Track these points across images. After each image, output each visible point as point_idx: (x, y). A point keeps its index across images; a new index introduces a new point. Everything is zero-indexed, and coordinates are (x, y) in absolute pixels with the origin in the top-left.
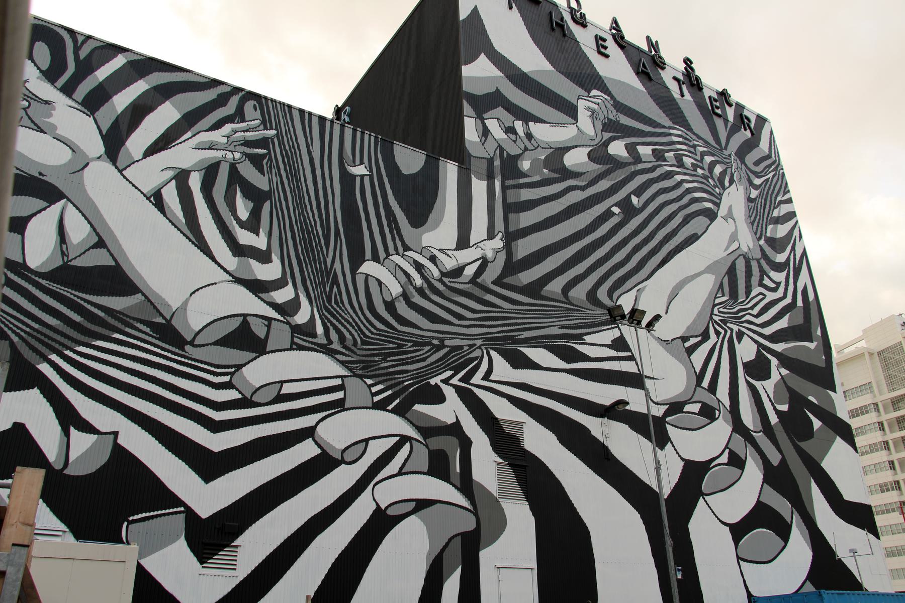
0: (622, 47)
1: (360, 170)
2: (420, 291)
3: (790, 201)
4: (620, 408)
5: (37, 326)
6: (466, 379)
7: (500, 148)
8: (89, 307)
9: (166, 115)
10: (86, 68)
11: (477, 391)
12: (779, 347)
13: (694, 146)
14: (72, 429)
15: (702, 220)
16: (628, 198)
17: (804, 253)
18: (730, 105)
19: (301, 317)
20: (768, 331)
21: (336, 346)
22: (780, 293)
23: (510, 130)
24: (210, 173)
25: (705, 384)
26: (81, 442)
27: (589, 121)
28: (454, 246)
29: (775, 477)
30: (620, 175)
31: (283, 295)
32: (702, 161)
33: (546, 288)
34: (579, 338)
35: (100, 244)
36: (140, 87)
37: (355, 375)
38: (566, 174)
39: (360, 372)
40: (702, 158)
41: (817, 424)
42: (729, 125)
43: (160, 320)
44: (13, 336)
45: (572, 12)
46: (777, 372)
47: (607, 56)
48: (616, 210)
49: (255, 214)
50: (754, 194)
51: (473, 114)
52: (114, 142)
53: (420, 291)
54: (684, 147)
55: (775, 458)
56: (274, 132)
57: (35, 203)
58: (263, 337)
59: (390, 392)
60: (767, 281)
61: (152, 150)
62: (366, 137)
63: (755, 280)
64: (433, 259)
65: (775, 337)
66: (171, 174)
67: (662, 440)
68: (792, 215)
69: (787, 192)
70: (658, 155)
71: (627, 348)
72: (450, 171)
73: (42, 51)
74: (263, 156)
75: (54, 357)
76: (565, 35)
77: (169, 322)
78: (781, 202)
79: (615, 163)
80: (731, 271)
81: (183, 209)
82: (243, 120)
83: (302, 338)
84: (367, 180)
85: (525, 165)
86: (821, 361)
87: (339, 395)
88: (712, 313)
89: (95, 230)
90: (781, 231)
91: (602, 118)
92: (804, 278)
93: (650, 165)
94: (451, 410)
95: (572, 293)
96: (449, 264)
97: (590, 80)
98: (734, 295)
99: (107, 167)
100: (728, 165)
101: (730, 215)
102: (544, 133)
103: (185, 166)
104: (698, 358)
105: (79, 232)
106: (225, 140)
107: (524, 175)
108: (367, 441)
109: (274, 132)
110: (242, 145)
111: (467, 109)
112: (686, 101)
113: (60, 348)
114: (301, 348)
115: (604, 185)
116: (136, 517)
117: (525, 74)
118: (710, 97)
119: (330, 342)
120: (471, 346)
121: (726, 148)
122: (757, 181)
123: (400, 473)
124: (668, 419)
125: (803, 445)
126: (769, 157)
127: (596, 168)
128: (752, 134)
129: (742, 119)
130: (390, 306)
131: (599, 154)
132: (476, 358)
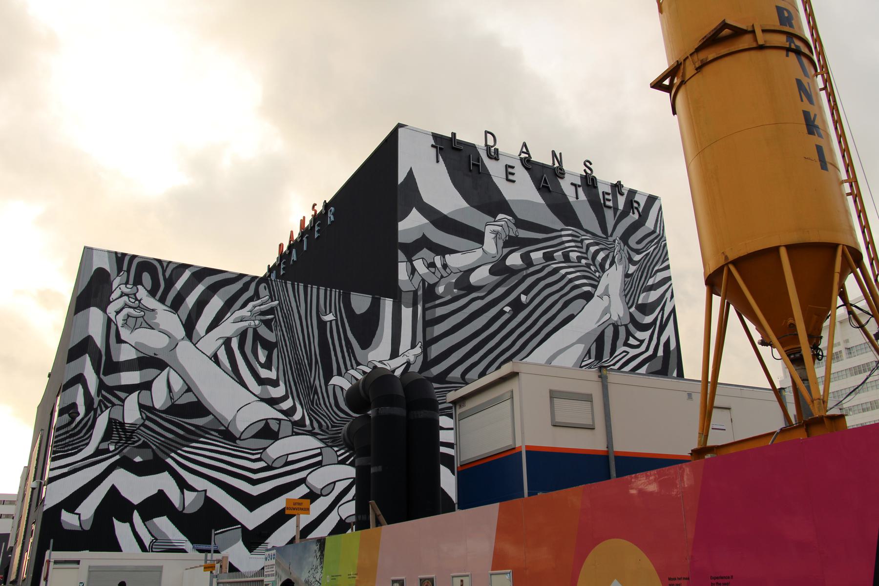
1: (329, 317)
7: (423, 281)
9: (216, 303)
10: (170, 283)
13: (582, 241)
15: (582, 301)
17: (673, 311)
19: (297, 417)
21: (317, 430)
22: (643, 348)
24: (243, 336)
26: (190, 496)
27: (493, 242)
31: (286, 405)
33: (450, 375)
35: (189, 390)
36: (200, 289)
37: (328, 446)
39: (330, 444)
40: (588, 249)
43: (223, 428)
48: (507, 309)
49: (269, 358)
50: (632, 269)
52: (189, 326)
54: (573, 244)
56: (277, 302)
57: (153, 372)
58: (276, 430)
61: (210, 329)
62: (333, 293)
66: (221, 341)
70: (548, 257)
72: (387, 305)
73: (146, 277)
75: (173, 455)
77: (227, 428)
79: (512, 271)
80: (600, 340)
82: (259, 298)
83: (298, 428)
84: (334, 323)
87: (319, 458)
91: (504, 236)
92: (669, 331)
98: (599, 356)
99: (187, 343)
101: (606, 293)
102: (456, 261)
103: (228, 335)
105: (178, 385)
106: (249, 314)
107: (440, 297)
108: (334, 483)
109: (277, 302)
111: (401, 256)
114: (298, 434)
115: (500, 291)
117: (445, 216)
119: (314, 429)
121: (611, 235)
122: (637, 258)
126: (654, 232)
127: (496, 279)
128: (640, 215)
131: (499, 268)
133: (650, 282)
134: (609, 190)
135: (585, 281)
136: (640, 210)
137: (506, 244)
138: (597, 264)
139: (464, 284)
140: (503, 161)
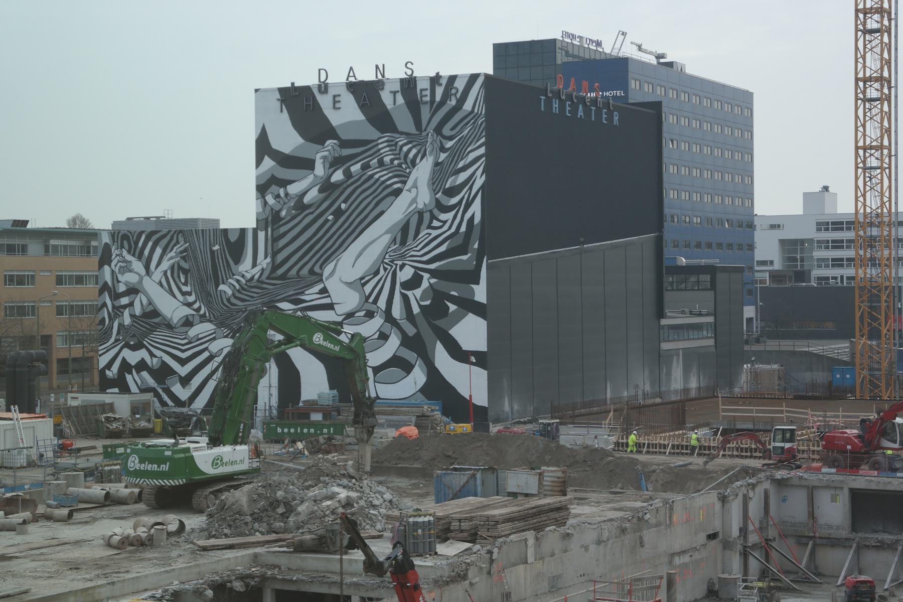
2: (239, 291)
7: (272, 209)
13: (396, 145)
19: (202, 312)
26: (155, 360)
29: (406, 341)
31: (196, 306)
34: (303, 293)
35: (150, 304)
53: (239, 291)
57: (133, 296)
64: (243, 276)
70: (365, 167)
79: (336, 186)
83: (203, 319)
95: (301, 273)
96: (248, 276)
101: (415, 186)
104: (368, 289)
121: (425, 130)
130: (228, 300)
131: (327, 187)
133: (461, 165)
134: (426, 85)
135: (396, 180)
136: (458, 95)
137: (331, 166)
138: (409, 161)
139: (300, 206)
140: (332, 92)
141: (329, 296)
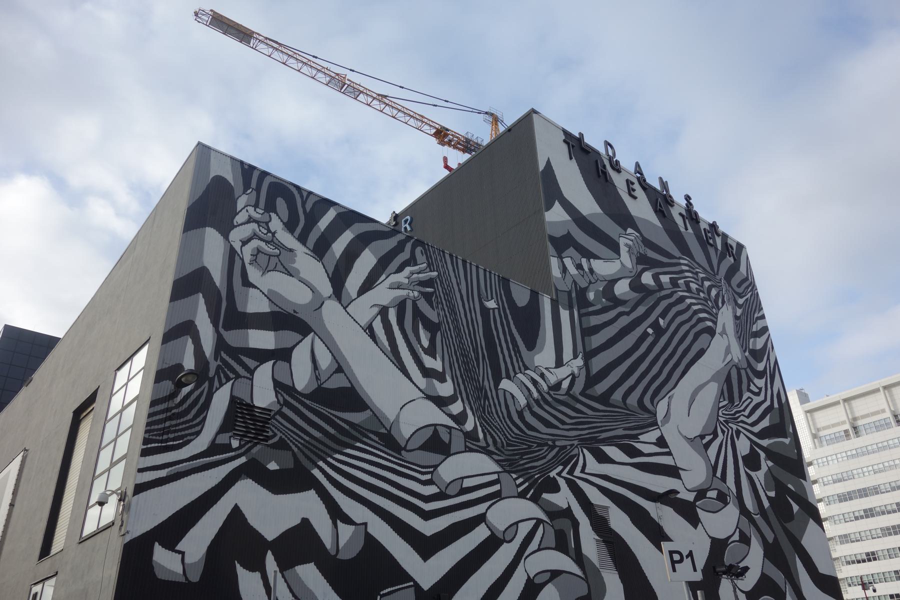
0: (644, 189)
1: (491, 304)
2: (537, 401)
3: (763, 317)
4: (672, 496)
5: (307, 438)
6: (571, 472)
8: (338, 421)
10: (312, 219)
11: (579, 482)
12: (765, 443)
13: (697, 273)
14: (338, 521)
15: (705, 337)
16: (657, 321)
17: (776, 362)
18: (718, 235)
19: (469, 426)
20: (756, 429)
21: (492, 448)
23: (579, 267)
25: (719, 474)
26: (346, 532)
28: (554, 366)
29: (773, 553)
30: (650, 301)
31: (456, 408)
32: (702, 286)
35: (339, 370)
36: (347, 237)
37: (505, 471)
38: (617, 302)
39: (508, 468)
40: (703, 283)
41: (796, 508)
42: (719, 253)
43: (383, 431)
44: (293, 447)
45: (610, 159)
46: (766, 464)
47: (635, 198)
48: (650, 331)
49: (432, 341)
50: (739, 312)
51: (555, 254)
53: (537, 401)
55: (770, 538)
56: (435, 273)
59: (527, 484)
60: (753, 387)
63: (744, 386)
64: (542, 376)
65: (762, 434)
67: (694, 521)
68: (765, 329)
69: (761, 309)
71: (666, 446)
74: (431, 294)
75: (321, 463)
76: (607, 181)
77: (389, 431)
78: (758, 318)
80: (728, 380)
81: (388, 340)
82: (416, 264)
83: (471, 442)
84: (496, 311)
85: (591, 296)
86: (793, 455)
87: (497, 487)
88: (718, 416)
89: (335, 358)
90: (759, 343)
93: (668, 292)
94: (563, 498)
95: (629, 401)
96: (553, 380)
97: (625, 220)
98: (731, 400)
100: (719, 287)
101: (724, 332)
104: (712, 451)
105: (325, 360)
107: (591, 304)
108: (517, 523)
110: (418, 285)
111: (551, 250)
112: (688, 233)
113: (324, 455)
114: (471, 450)
115: (641, 310)
116: (385, 592)
118: (705, 229)
119: (488, 445)
120: (572, 445)
123: (539, 550)
124: (697, 503)
125: (788, 525)
126: (746, 279)
128: (735, 260)
129: (726, 246)
131: (636, 285)
132: (575, 456)
141: (669, 454)
